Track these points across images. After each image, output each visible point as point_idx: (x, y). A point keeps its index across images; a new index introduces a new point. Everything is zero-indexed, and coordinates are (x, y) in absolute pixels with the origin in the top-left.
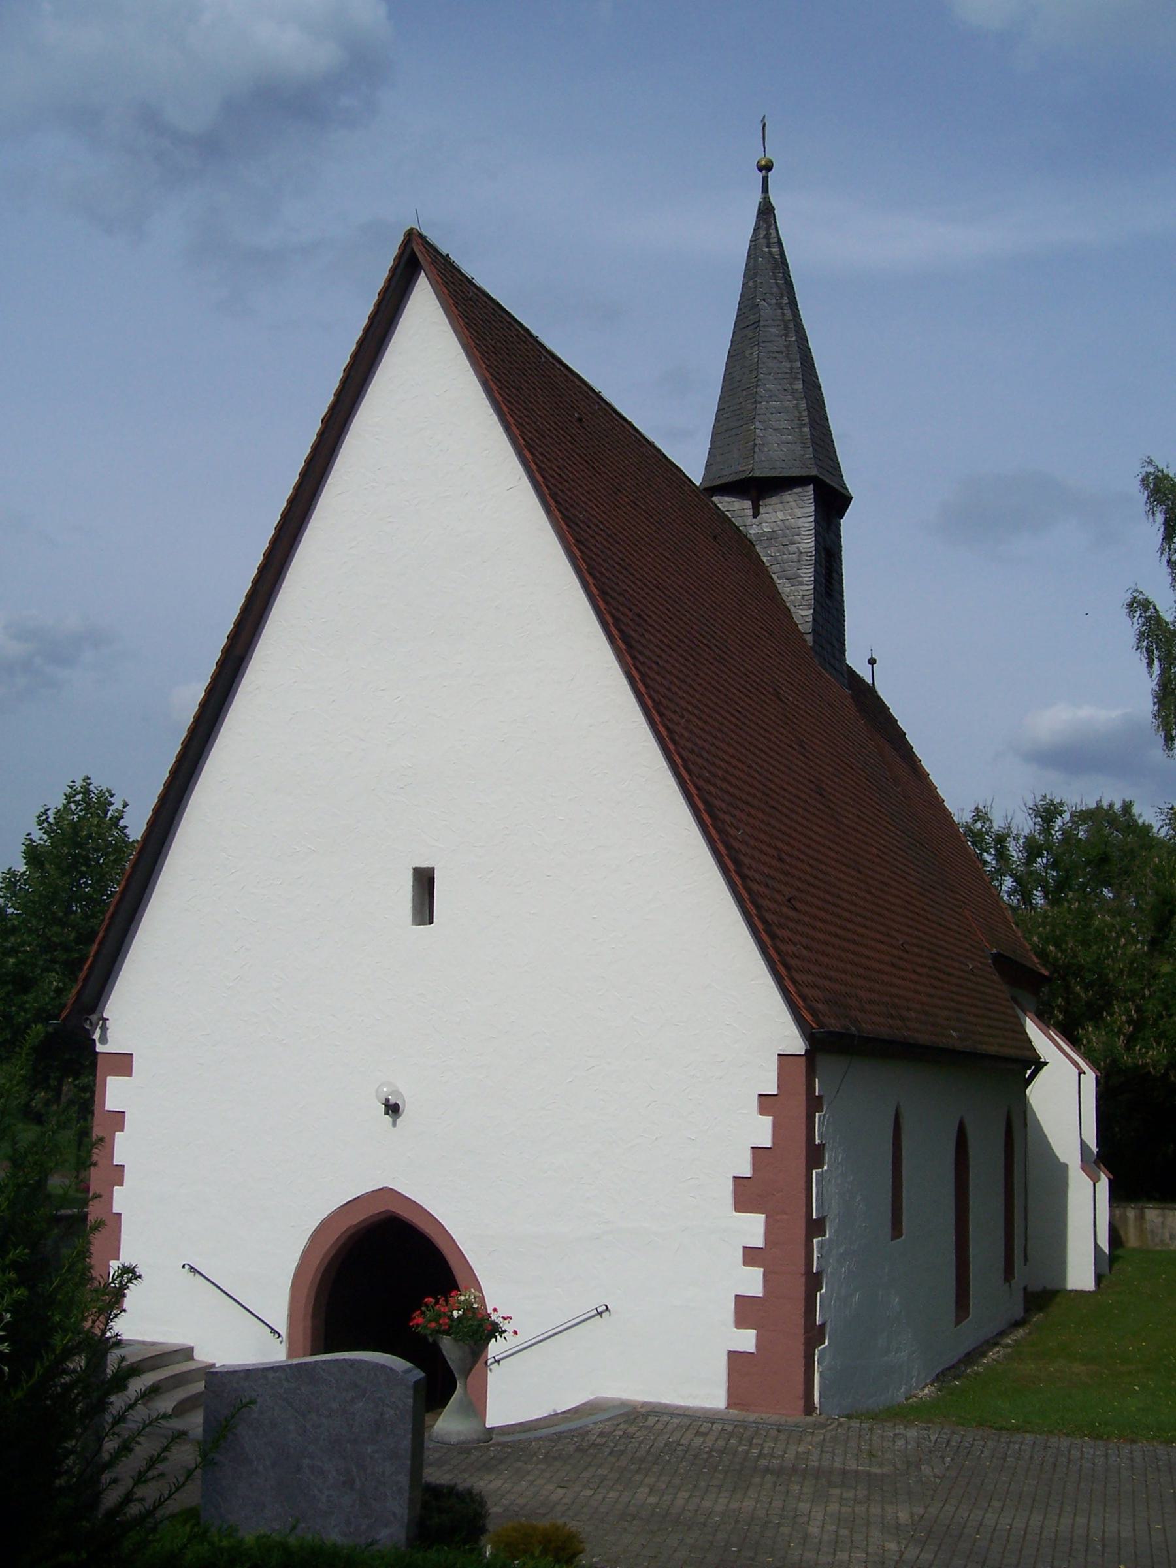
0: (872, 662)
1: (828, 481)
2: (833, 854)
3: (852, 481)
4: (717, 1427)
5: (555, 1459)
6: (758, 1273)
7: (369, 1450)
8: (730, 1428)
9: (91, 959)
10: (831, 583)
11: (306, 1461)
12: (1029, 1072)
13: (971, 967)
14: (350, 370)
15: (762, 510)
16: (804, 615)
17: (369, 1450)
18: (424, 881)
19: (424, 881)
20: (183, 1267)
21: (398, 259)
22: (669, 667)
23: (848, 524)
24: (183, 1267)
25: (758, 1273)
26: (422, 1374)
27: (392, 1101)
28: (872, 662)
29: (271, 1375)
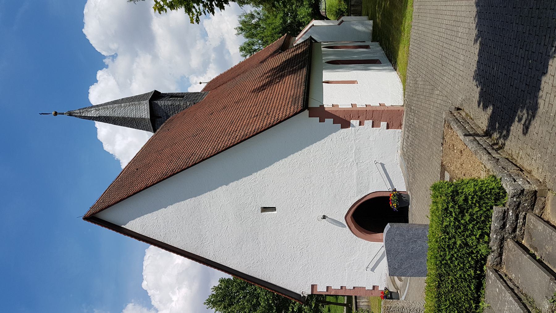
0: (201, 83)
1: (150, 97)
2: (255, 99)
3: (150, 90)
4: (406, 132)
5: (414, 176)
6: (366, 122)
7: (407, 237)
8: (407, 130)
9: (287, 297)
10: (180, 96)
11: (410, 252)
12: (313, 41)
13: (284, 58)
14: (125, 234)
15: (160, 116)
16: (231, 277)
17: (407, 237)
18: (265, 209)
19: (265, 209)
20: (367, 270)
21: (92, 222)
22: (206, 147)
23: (162, 91)
24: (367, 270)
25: (366, 122)
26: (388, 224)
27: (322, 217)
28: (201, 83)
29: (389, 260)
